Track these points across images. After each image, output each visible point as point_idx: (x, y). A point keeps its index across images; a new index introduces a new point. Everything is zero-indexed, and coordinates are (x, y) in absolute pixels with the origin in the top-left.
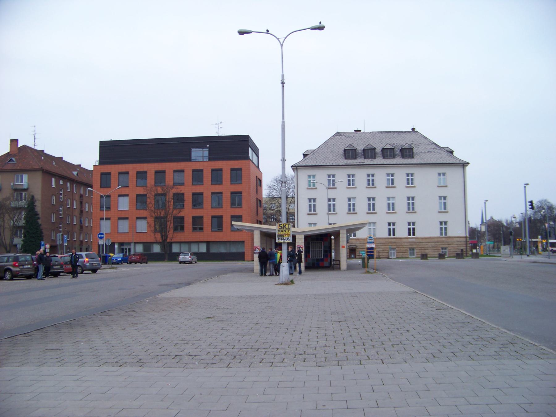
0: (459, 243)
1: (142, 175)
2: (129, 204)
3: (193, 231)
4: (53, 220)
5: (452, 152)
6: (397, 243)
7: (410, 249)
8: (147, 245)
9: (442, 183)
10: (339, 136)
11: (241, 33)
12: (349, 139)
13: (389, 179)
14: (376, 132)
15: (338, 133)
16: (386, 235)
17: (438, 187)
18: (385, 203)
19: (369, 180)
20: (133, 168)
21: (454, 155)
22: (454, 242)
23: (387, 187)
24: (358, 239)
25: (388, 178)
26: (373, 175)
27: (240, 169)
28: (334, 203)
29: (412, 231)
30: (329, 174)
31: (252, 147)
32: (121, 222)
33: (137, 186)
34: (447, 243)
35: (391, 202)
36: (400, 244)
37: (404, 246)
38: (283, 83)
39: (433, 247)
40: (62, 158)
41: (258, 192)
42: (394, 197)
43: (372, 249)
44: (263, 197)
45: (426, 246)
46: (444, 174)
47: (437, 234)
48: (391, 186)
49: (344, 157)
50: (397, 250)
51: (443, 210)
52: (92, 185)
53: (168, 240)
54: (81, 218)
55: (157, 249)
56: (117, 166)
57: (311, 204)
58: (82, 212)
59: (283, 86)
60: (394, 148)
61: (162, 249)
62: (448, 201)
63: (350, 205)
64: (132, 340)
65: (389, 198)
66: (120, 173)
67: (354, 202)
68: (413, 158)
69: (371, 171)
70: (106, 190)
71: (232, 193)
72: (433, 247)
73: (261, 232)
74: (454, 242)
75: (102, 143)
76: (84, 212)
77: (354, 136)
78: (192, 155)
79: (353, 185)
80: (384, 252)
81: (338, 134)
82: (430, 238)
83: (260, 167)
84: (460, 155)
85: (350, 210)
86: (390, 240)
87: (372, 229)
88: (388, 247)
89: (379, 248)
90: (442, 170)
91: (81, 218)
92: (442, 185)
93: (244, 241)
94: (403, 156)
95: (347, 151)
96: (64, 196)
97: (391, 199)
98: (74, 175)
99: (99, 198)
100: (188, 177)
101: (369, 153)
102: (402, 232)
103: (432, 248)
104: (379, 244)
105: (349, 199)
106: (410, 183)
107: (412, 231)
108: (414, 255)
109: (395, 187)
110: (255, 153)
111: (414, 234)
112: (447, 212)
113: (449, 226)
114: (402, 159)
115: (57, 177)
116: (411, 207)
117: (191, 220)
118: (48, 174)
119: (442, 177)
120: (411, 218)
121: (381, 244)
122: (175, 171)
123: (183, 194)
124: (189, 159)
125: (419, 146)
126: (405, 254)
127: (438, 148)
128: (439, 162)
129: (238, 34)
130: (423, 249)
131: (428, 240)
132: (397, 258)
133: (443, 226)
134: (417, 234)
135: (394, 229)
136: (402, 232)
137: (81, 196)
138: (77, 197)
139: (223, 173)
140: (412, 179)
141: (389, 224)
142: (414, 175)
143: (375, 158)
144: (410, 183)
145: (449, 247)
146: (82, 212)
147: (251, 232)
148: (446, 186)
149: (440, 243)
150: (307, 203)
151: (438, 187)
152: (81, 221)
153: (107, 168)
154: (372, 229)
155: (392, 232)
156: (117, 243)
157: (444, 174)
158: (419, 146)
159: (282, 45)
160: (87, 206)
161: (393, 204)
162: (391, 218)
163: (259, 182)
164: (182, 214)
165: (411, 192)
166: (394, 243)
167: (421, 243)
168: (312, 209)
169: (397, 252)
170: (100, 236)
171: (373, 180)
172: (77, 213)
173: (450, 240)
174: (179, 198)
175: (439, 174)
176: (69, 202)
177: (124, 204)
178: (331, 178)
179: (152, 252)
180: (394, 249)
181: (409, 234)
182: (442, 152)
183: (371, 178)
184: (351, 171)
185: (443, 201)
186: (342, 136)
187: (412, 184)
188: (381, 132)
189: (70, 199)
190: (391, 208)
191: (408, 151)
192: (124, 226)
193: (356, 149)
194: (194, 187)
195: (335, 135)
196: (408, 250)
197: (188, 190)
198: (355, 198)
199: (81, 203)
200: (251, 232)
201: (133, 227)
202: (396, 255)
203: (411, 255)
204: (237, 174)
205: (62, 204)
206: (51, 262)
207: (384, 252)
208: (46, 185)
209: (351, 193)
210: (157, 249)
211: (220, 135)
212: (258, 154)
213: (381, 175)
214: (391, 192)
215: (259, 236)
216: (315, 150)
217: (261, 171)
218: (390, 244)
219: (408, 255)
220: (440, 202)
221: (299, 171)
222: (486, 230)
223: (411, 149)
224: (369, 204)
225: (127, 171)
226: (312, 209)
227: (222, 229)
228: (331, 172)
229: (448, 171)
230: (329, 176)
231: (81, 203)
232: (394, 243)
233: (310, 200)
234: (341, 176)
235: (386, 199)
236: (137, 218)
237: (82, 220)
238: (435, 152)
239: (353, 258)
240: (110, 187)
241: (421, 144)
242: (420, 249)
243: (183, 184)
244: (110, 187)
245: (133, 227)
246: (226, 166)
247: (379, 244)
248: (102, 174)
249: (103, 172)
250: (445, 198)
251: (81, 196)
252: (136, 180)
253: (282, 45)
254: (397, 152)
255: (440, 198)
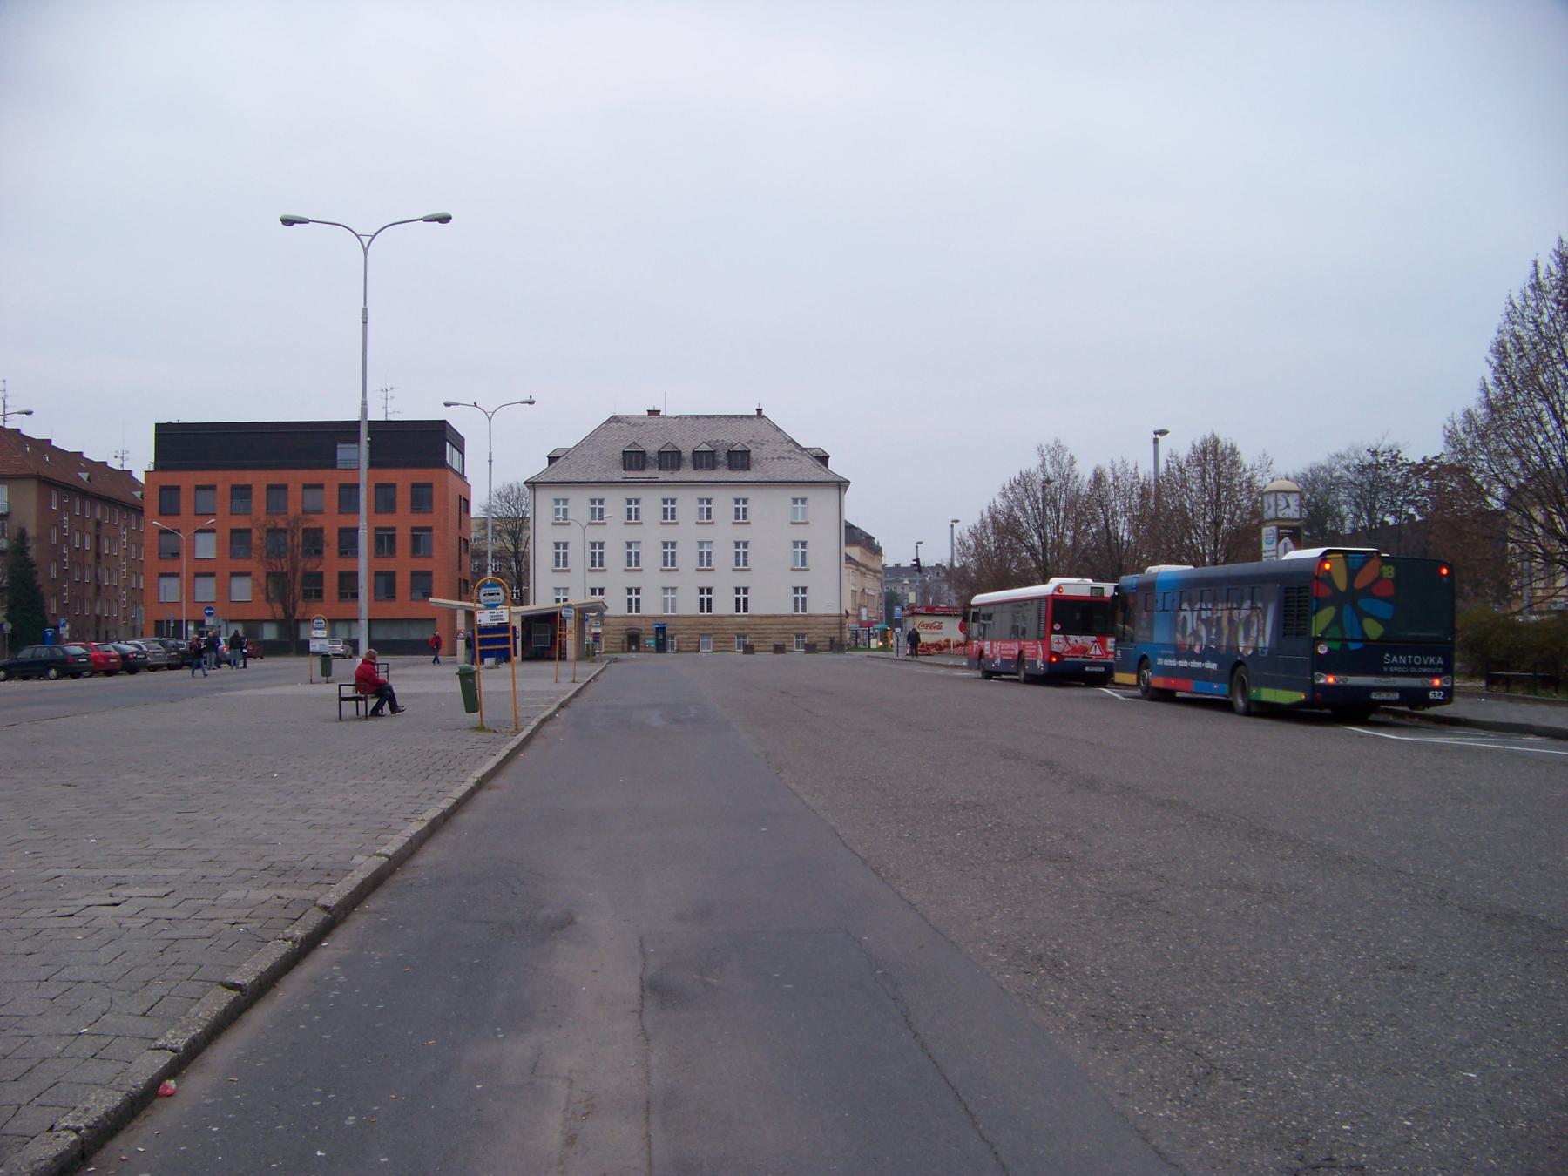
0: (827, 626)
1: (241, 492)
2: (217, 546)
3: (339, 601)
4: (54, 576)
5: (823, 459)
6: (715, 625)
7: (739, 637)
8: (253, 625)
9: (799, 517)
10: (617, 422)
11: (288, 222)
12: (635, 429)
13: (703, 508)
14: (686, 417)
15: (614, 417)
16: (695, 610)
17: (792, 523)
18: (696, 550)
19: (665, 510)
20: (224, 479)
21: (829, 468)
22: (819, 624)
23: (697, 523)
24: (644, 617)
25: (701, 506)
26: (673, 502)
27: (430, 486)
28: (601, 550)
29: (742, 604)
30: (592, 497)
31: (452, 442)
32: (200, 582)
33: (231, 514)
34: (805, 627)
35: (705, 550)
36: (719, 627)
37: (728, 631)
38: (490, 461)
39: (781, 633)
40: (49, 441)
41: (462, 526)
42: (711, 542)
43: (598, 634)
44: (472, 516)
45: (769, 631)
46: (803, 501)
47: (789, 610)
48: (705, 520)
49: (622, 467)
50: (714, 638)
51: (800, 567)
52: (142, 508)
53: (296, 618)
54: (96, 568)
55: (270, 633)
56: (191, 473)
57: (559, 553)
58: (98, 556)
59: (490, 464)
60: (715, 451)
61: (280, 635)
62: (810, 550)
63: (629, 555)
64: (141, 846)
65: (701, 544)
66: (199, 488)
67: (637, 550)
68: (749, 469)
69: (669, 493)
70: (171, 519)
71: (414, 529)
72: (781, 633)
73: (466, 611)
74: (819, 624)
75: (160, 428)
76: (103, 556)
77: (644, 423)
78: (339, 458)
79: (636, 519)
80: (691, 640)
81: (615, 419)
82: (775, 616)
83: (466, 475)
84: (836, 467)
85: (629, 564)
86: (702, 620)
87: (670, 600)
88: (696, 631)
89: (682, 634)
90: (798, 493)
91: (96, 568)
92: (799, 521)
93: (435, 619)
94: (732, 467)
95: (627, 454)
96: (71, 525)
97: (705, 545)
98: (136, 498)
99: (157, 534)
100: (330, 498)
101: (670, 459)
102: (724, 605)
103: (778, 635)
104: (682, 627)
105: (629, 545)
106: (741, 516)
107: (742, 604)
108: (708, 648)
109: (712, 523)
110: (456, 448)
111: (746, 610)
112: (807, 570)
113: (809, 595)
114: (729, 472)
115: (60, 489)
116: (741, 560)
117: (336, 580)
118: (46, 483)
119: (799, 505)
120: (742, 580)
121: (686, 627)
122: (306, 487)
123: (321, 530)
124: (333, 466)
125: (763, 445)
126: (731, 644)
127: (797, 450)
128: (795, 479)
129: (444, 406)
130: (761, 636)
131: (770, 621)
132: (714, 652)
133: (800, 595)
134: (752, 610)
135: (709, 600)
136: (724, 605)
137: (98, 524)
138: (91, 527)
139: (398, 493)
140: (745, 509)
141: (701, 591)
142: (748, 502)
143: (678, 469)
144: (741, 516)
145: (809, 633)
146: (98, 556)
147: (453, 613)
148: (807, 523)
149: (792, 627)
150: (552, 551)
151: (792, 523)
152: (96, 575)
153: (171, 478)
154: (670, 600)
155: (706, 604)
156: (191, 621)
157: (803, 501)
158: (763, 445)
159: (366, 251)
160: (106, 544)
161: (709, 554)
162: (705, 580)
163: (465, 503)
164: (320, 569)
165: (742, 533)
166: (710, 625)
167: (759, 625)
168: (561, 561)
169: (714, 642)
170: (207, 611)
171: (673, 510)
172: (91, 560)
173: (811, 621)
174: (314, 539)
175: (795, 501)
176: (77, 537)
177: (207, 548)
178: (597, 506)
179: (260, 639)
180: (709, 635)
181: (738, 610)
182: (806, 459)
183: (669, 506)
184: (633, 493)
185: (800, 549)
186: (622, 422)
187: (745, 518)
188: (697, 417)
189: (80, 531)
190: (705, 561)
191: (739, 456)
192: (206, 590)
193: (644, 453)
194: (343, 517)
195: (609, 421)
196: (792, 638)
197: (331, 524)
198: (639, 542)
199: (98, 538)
200: (453, 613)
201: (224, 591)
202: (714, 647)
203: (798, 647)
204: (422, 497)
205: (67, 541)
206: (960, 624)
207: (691, 640)
208: (44, 504)
209: (632, 533)
210: (270, 633)
211: (392, 418)
212: (463, 449)
213: (687, 503)
214: (705, 533)
215: (464, 616)
216: (571, 449)
217: (468, 482)
218: (702, 627)
219: (734, 646)
220: (795, 552)
221: (538, 493)
222: (917, 600)
223: (746, 453)
224: (665, 554)
225: (213, 483)
226: (561, 561)
227: (394, 597)
228: (597, 493)
229: (811, 494)
230: (593, 502)
231: (98, 538)
232: (710, 625)
233: (557, 545)
234: (615, 502)
235: (697, 545)
236: (233, 574)
237: (99, 572)
238: (790, 459)
239: (634, 651)
240: (179, 514)
241: (768, 441)
242: (757, 636)
243: (321, 512)
244: (179, 514)
245: (224, 591)
246: (404, 479)
247: (682, 627)
248: (162, 489)
249: (164, 484)
250: (804, 544)
251: (98, 524)
252: (230, 501)
253: (366, 251)
254: (722, 457)
255: (795, 544)
